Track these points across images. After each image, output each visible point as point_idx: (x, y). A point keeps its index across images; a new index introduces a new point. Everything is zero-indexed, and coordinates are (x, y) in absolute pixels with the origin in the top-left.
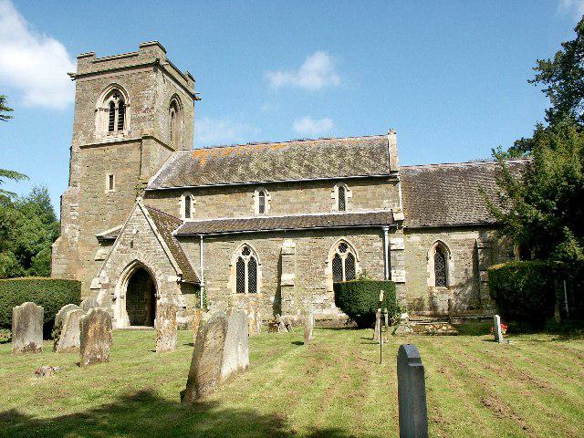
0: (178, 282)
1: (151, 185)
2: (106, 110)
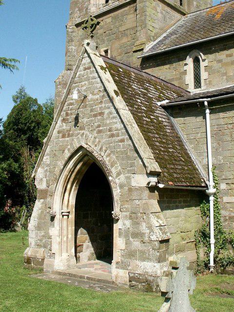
0: (152, 189)
1: (148, 49)
2: (197, 61)
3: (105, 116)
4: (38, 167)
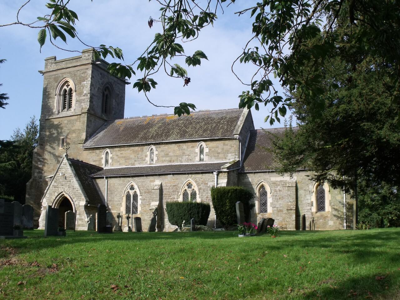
3: (71, 182)
4: (44, 198)
